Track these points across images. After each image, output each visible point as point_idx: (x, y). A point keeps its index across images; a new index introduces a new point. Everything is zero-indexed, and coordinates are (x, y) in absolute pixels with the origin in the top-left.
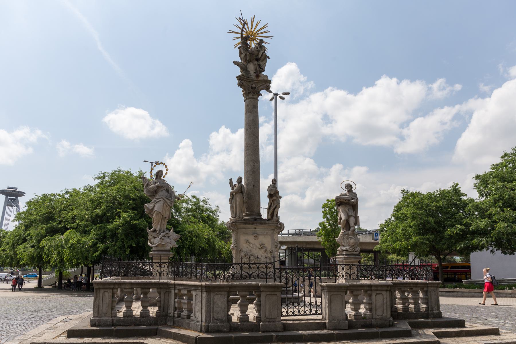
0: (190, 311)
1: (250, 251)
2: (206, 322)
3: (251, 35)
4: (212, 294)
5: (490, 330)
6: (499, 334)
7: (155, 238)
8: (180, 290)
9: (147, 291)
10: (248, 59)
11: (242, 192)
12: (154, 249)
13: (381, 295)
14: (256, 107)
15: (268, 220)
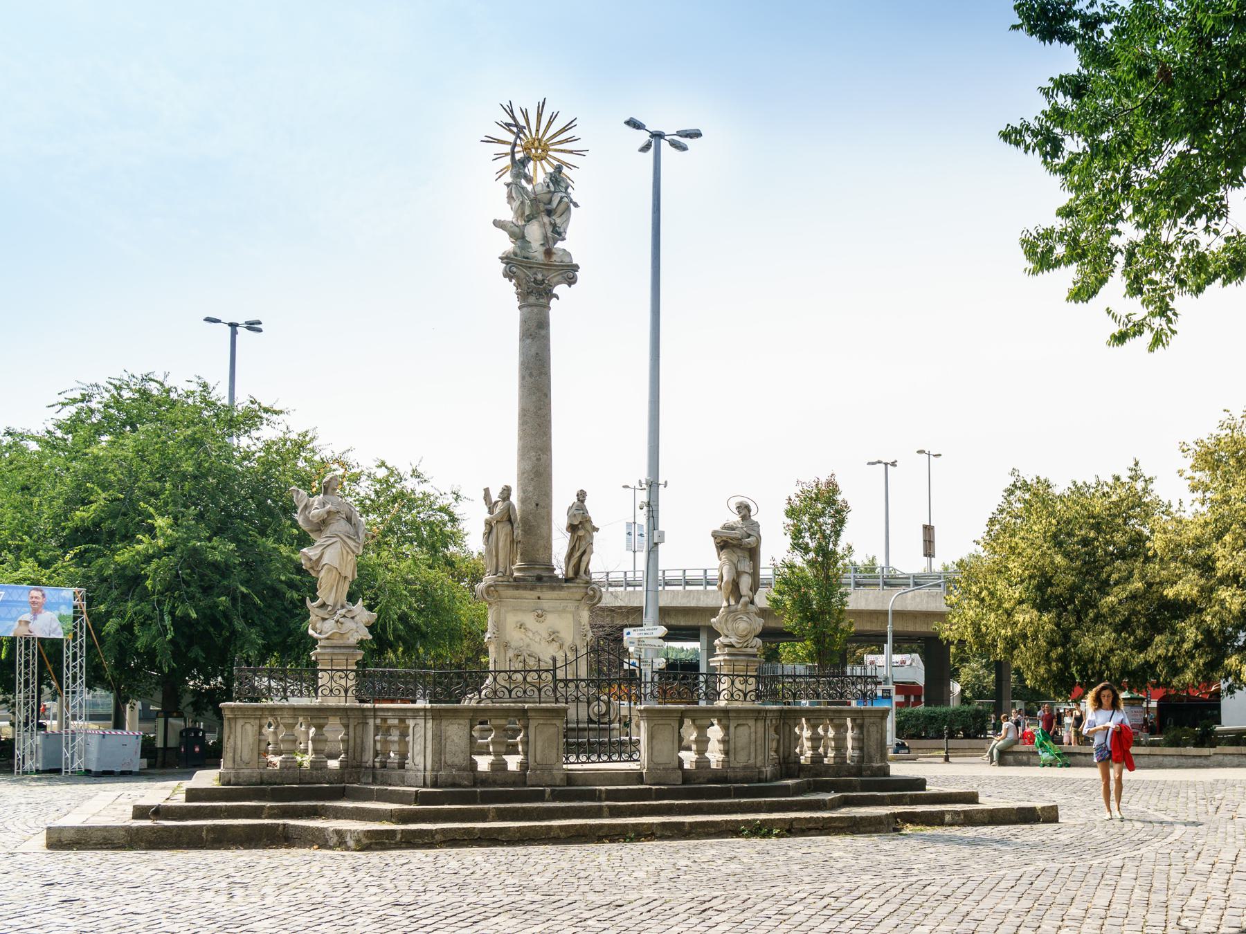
0: (403, 756)
1: (528, 645)
2: (433, 770)
3: (536, 149)
4: (444, 723)
7: (324, 619)
8: (384, 720)
9: (322, 721)
10: (527, 213)
11: (510, 520)
13: (746, 727)
15: (567, 580)
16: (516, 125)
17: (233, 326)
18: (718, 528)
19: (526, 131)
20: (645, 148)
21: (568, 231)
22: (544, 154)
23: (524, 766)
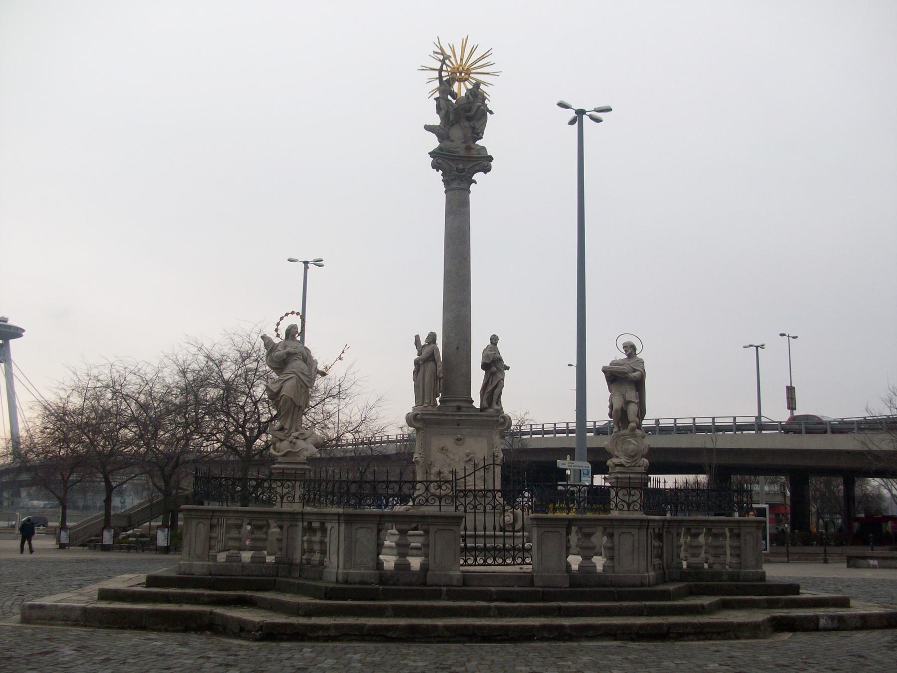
0: (323, 552)
5: (833, 599)
6: (849, 607)
7: (281, 440)
14: (465, 204)
16: (443, 53)
17: (306, 263)
18: (608, 365)
19: (452, 59)
20: (572, 122)
22: (467, 76)
23: (424, 568)
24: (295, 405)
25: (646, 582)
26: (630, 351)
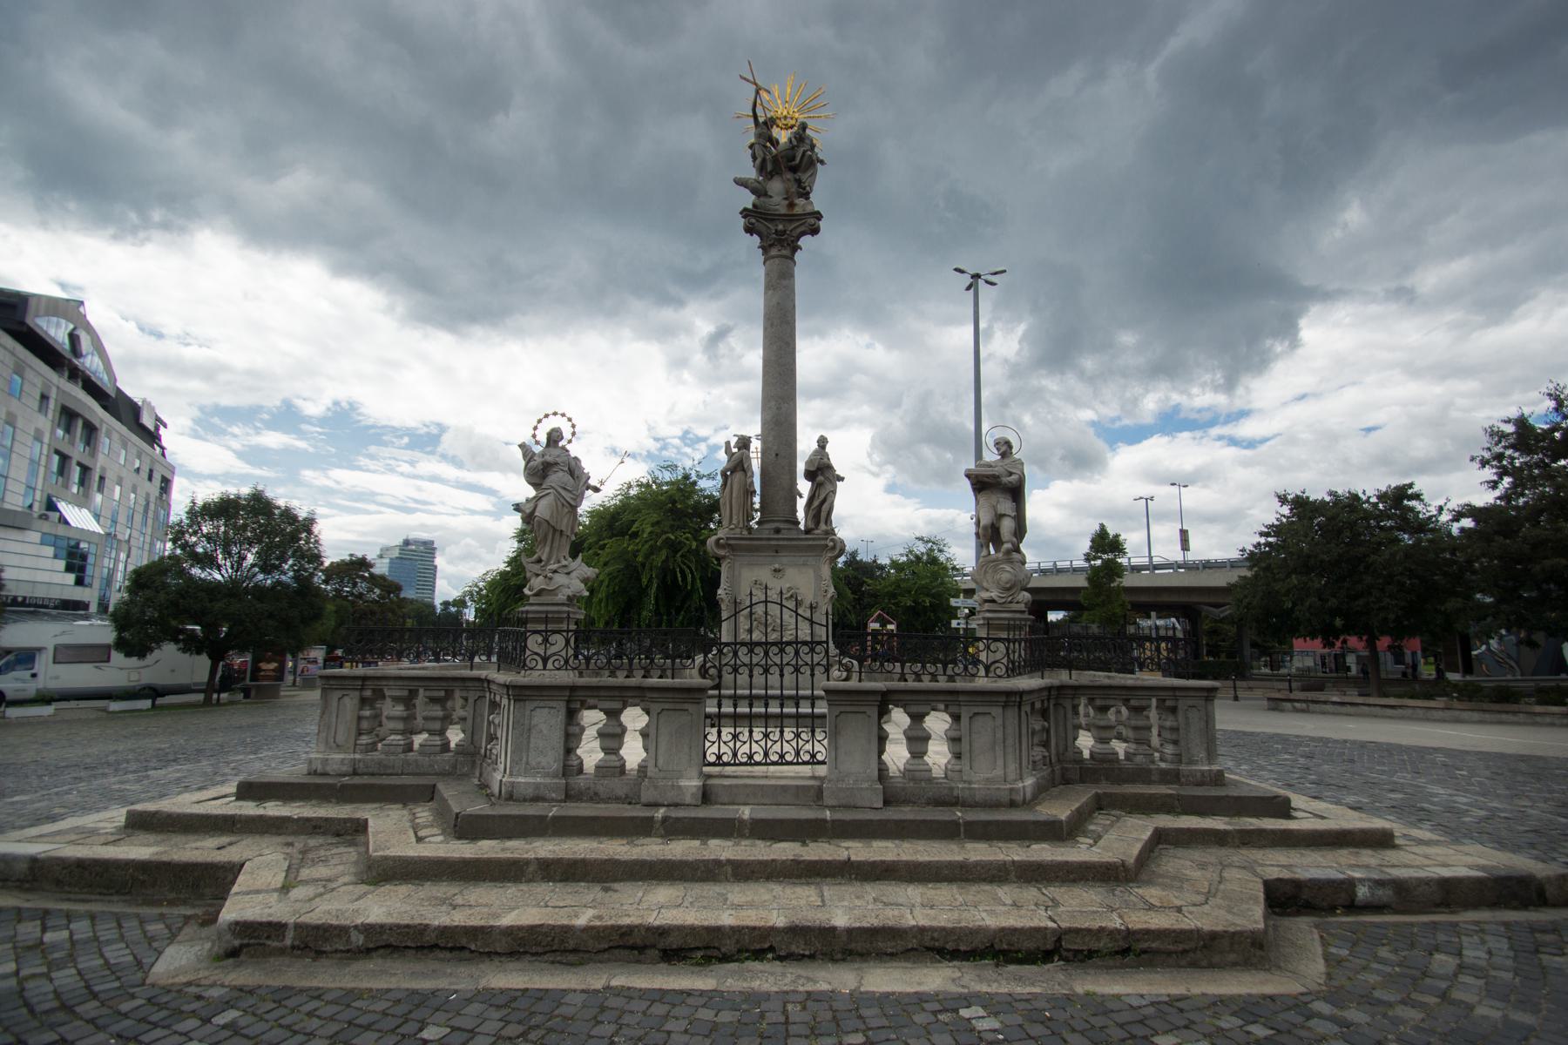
4: (529, 705)
12: (532, 600)
20: (968, 288)
21: (815, 188)
24: (555, 530)
25: (1019, 798)
26: (1004, 448)
